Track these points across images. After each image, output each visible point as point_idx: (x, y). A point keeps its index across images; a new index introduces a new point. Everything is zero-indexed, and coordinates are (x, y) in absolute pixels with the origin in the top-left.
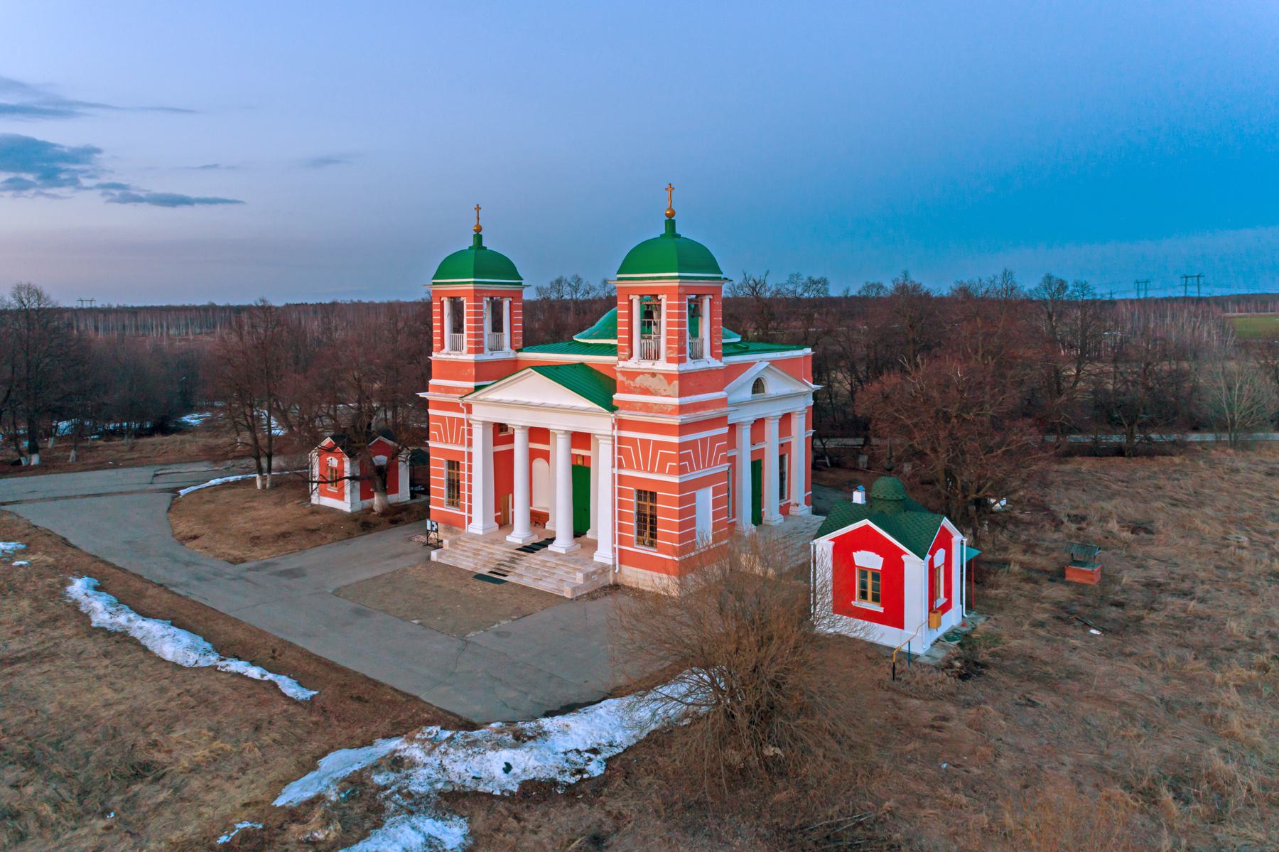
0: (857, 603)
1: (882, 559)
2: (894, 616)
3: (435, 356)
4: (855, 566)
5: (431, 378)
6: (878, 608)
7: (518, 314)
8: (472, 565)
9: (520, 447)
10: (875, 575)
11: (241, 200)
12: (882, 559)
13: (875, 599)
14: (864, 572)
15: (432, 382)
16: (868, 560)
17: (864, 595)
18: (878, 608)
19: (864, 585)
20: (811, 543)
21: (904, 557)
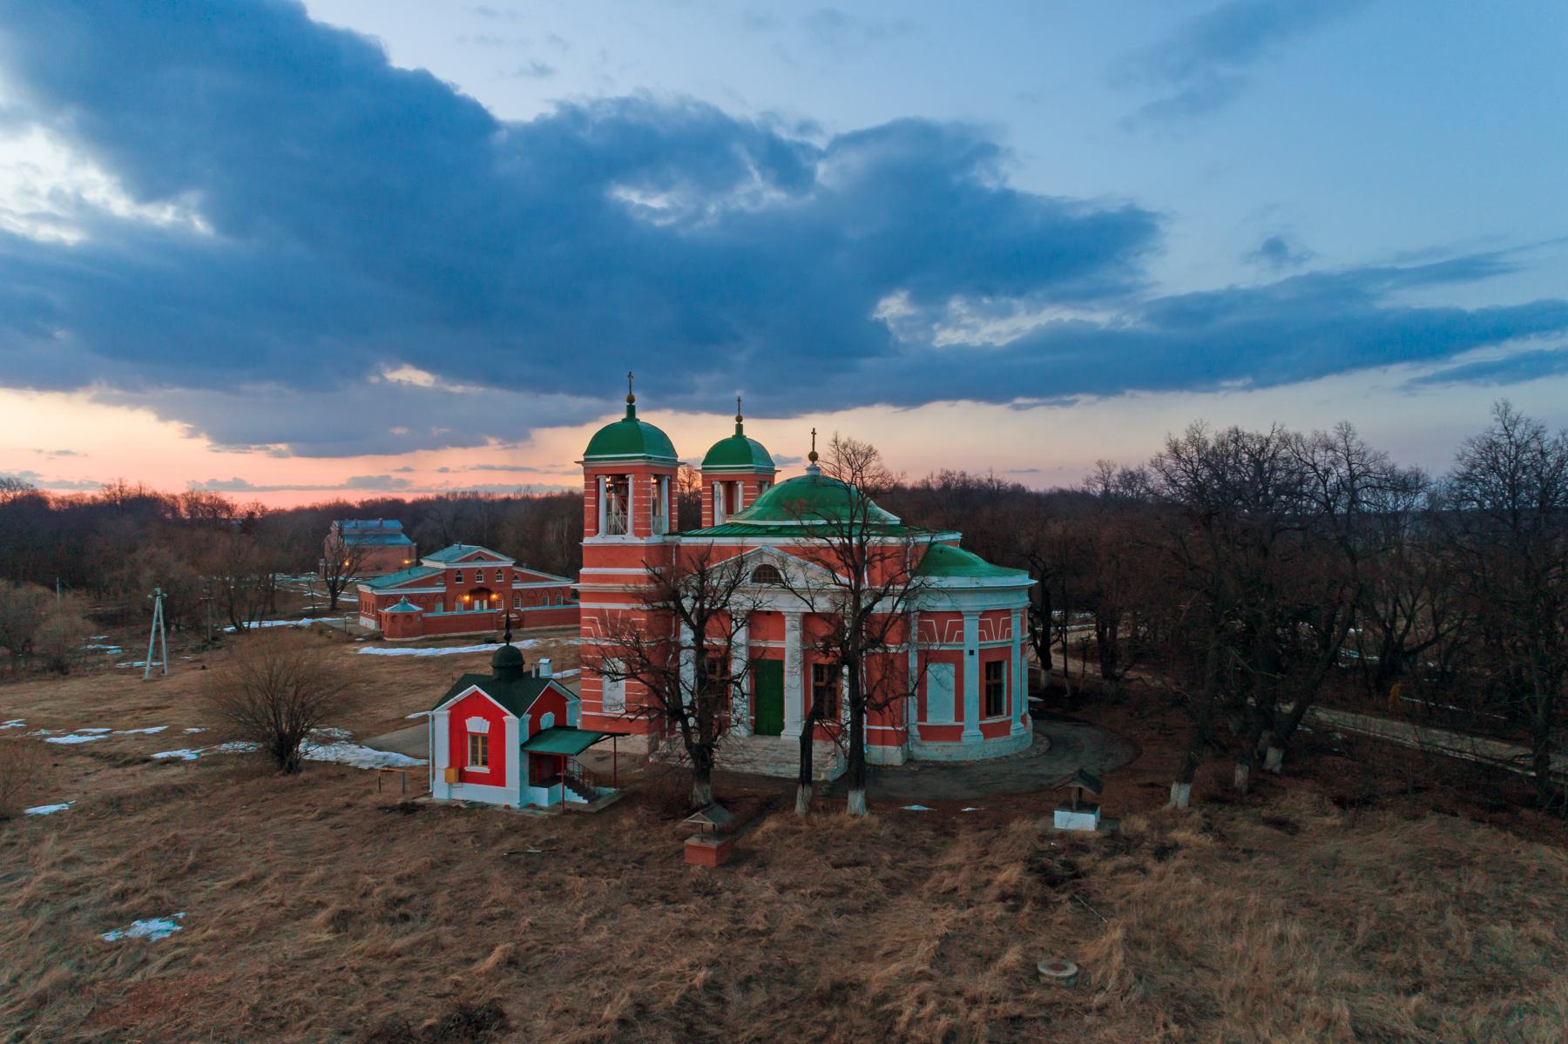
0: (469, 769)
1: (488, 723)
2: (497, 778)
3: (587, 541)
4: (465, 732)
5: (581, 567)
6: (485, 770)
7: (707, 516)
8: (757, 742)
9: (993, 689)
10: (485, 738)
11: (796, 455)
12: (488, 723)
13: (485, 763)
14: (475, 736)
15: (583, 571)
16: (477, 725)
17: (475, 761)
18: (485, 770)
19: (475, 751)
20: (1020, 728)
21: (505, 718)
